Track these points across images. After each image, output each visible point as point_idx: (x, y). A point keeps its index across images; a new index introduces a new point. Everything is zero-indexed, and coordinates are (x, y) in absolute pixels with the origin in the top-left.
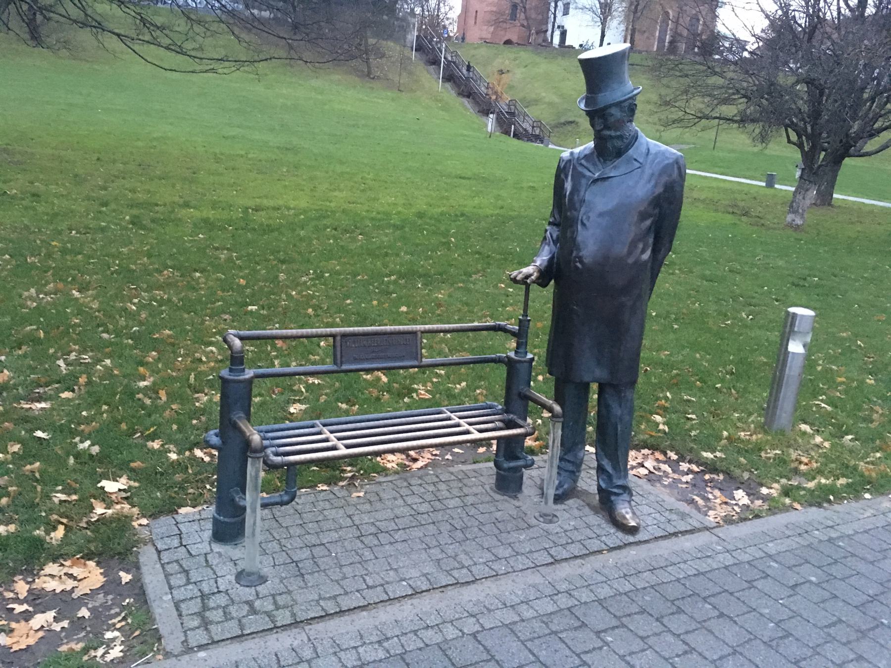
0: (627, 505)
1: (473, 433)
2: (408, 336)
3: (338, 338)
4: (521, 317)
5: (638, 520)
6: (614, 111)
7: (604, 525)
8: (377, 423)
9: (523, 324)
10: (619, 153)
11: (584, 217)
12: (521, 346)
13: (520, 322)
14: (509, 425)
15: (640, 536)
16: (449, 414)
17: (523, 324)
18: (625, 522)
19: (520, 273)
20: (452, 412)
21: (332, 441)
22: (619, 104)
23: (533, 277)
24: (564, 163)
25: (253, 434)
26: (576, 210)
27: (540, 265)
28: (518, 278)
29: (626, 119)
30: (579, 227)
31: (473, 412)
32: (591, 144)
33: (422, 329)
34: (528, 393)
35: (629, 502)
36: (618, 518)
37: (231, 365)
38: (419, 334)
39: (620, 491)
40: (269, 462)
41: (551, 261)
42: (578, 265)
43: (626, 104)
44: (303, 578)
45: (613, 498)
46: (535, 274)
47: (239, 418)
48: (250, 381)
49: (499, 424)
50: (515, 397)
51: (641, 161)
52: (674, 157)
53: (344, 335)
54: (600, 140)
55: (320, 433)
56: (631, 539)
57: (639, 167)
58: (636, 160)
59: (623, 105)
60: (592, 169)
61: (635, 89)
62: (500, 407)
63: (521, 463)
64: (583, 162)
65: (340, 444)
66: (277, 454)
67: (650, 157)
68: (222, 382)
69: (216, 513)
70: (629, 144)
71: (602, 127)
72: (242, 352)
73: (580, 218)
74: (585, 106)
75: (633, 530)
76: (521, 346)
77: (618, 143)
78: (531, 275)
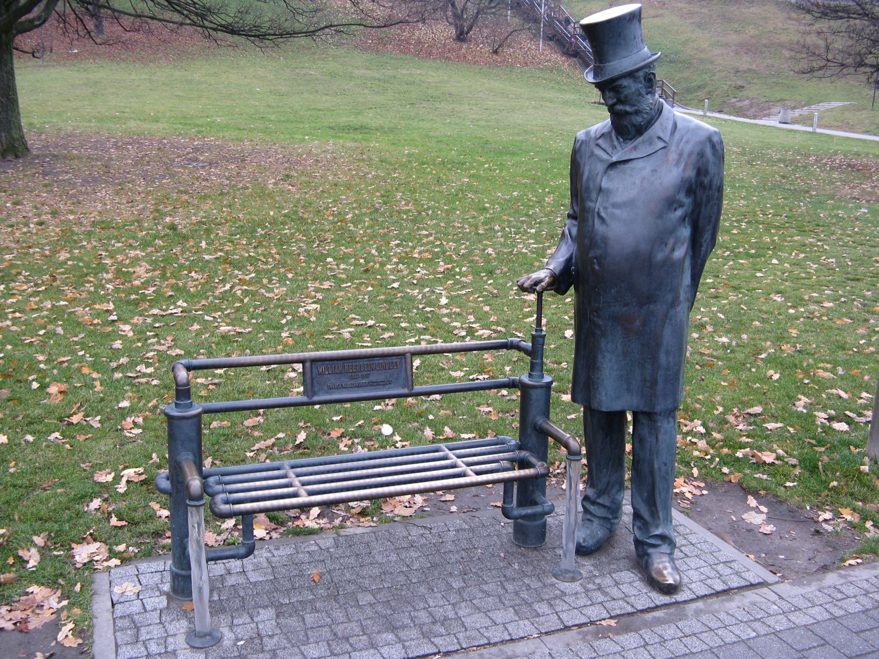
0: (665, 558)
1: (469, 476)
2: (394, 360)
3: (308, 364)
4: (534, 333)
5: (678, 577)
6: (625, 82)
7: (638, 584)
8: (316, 468)
9: (538, 340)
10: (640, 130)
11: (601, 210)
12: (536, 367)
13: (534, 337)
14: (523, 464)
15: (680, 597)
16: (447, 451)
17: (538, 340)
18: (660, 579)
19: (528, 279)
20: (450, 450)
21: (460, 467)
22: (631, 74)
23: (543, 284)
24: (579, 144)
25: (194, 479)
26: (591, 201)
27: (555, 268)
28: (525, 285)
29: (643, 91)
30: (597, 222)
31: (478, 449)
32: (609, 121)
33: (412, 350)
34: (545, 426)
35: (671, 554)
36: (654, 575)
37: (177, 399)
38: (408, 355)
39: (659, 542)
40: (216, 510)
41: (568, 261)
42: (597, 267)
43: (641, 74)
44: (262, 641)
45: (651, 550)
46: (547, 279)
47: (187, 459)
48: (198, 416)
49: (505, 464)
50: (529, 431)
51: (667, 139)
52: (703, 136)
53: (314, 361)
54: (616, 116)
55: (445, 458)
56: (665, 599)
57: (664, 148)
58: (659, 138)
59: (637, 74)
60: (609, 150)
61: (653, 55)
62: (513, 442)
63: (538, 509)
64: (600, 141)
65: (468, 470)
66: (227, 502)
67: (677, 136)
68: (168, 418)
69: (174, 566)
70: (652, 119)
71: (615, 100)
72: (188, 384)
73: (596, 210)
74: (594, 78)
75: (670, 590)
76: (536, 367)
77: (638, 119)
78: (541, 281)
